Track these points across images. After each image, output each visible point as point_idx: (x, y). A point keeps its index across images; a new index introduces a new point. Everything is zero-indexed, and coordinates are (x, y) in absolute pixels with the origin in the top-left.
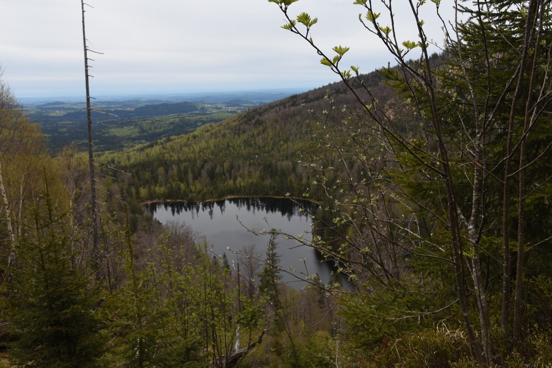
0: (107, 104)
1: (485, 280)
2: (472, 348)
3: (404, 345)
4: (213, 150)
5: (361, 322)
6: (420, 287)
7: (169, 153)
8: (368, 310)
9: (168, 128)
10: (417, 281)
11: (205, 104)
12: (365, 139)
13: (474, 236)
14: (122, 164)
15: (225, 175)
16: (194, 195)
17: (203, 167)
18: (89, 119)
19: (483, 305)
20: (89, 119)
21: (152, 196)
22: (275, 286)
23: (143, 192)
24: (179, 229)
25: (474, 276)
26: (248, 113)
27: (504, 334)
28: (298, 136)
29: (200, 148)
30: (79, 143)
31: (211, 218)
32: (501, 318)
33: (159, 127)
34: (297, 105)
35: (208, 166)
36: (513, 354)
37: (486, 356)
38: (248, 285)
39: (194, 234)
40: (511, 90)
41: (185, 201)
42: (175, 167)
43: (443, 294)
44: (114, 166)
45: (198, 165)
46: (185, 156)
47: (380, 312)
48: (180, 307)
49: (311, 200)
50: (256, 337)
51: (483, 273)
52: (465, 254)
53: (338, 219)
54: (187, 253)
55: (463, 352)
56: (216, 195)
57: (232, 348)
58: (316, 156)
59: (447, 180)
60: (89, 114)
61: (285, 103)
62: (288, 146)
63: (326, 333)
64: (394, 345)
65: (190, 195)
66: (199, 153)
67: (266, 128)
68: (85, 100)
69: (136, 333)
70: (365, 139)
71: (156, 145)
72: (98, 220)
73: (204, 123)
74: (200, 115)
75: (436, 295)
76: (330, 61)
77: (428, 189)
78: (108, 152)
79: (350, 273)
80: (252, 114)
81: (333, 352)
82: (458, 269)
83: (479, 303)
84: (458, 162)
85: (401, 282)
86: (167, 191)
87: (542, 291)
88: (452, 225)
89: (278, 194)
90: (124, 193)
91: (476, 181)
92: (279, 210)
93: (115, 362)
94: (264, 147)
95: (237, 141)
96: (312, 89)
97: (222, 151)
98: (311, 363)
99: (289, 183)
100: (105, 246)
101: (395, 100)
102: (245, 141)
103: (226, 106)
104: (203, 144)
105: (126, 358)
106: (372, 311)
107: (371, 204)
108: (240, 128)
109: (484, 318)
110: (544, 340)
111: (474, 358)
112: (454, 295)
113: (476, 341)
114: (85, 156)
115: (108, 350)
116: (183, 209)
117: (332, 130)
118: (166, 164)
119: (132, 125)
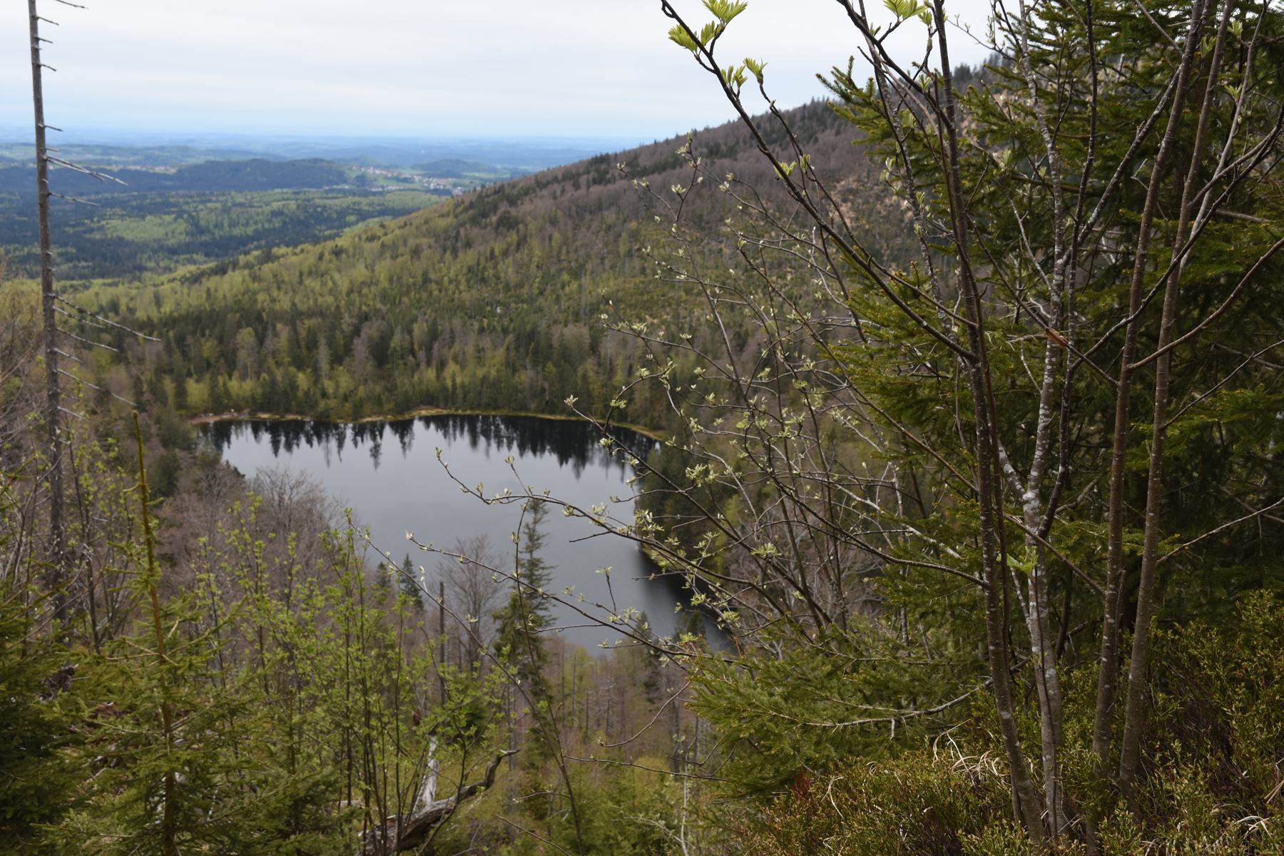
0: (98, 151)
1: (1059, 635)
2: (1019, 800)
3: (849, 791)
4: (384, 290)
5: (748, 728)
6: (897, 648)
7: (268, 290)
8: (765, 698)
9: (267, 225)
10: (890, 635)
11: (368, 166)
12: (779, 277)
13: (1037, 519)
14: (141, 315)
15: (414, 356)
16: (333, 403)
17: (357, 331)
18: (43, 185)
19: (1051, 692)
20: (43, 185)
21: (218, 402)
22: (535, 642)
23: (197, 390)
24: (288, 491)
25: (1031, 620)
26: (480, 197)
27: (1098, 766)
28: (607, 263)
29: (351, 282)
30: (17, 253)
31: (376, 464)
32: (1093, 725)
33: (242, 221)
34: (609, 181)
35: (371, 331)
36: (1116, 816)
37: (1051, 819)
38: (465, 638)
39: (329, 505)
40: (1144, 152)
41: (307, 419)
42: (283, 331)
43: (953, 667)
44: (117, 319)
45: (344, 327)
46: (311, 302)
47: (794, 705)
48: (282, 690)
49: (635, 428)
50: (478, 771)
51: (1053, 616)
52: (1011, 561)
53: (699, 468)
54: (308, 554)
55: (996, 810)
56: (391, 405)
57: (414, 798)
58: (651, 316)
59: (978, 369)
60: (43, 171)
61: (579, 175)
62: (580, 286)
63: (659, 764)
64: (828, 792)
65: (322, 404)
66: (348, 294)
67: (525, 237)
68: (33, 138)
69: (159, 758)
70: (779, 277)
71: (234, 269)
72: (65, 460)
73: (363, 216)
74: (354, 194)
75: (935, 668)
76: (693, 37)
77: (931, 400)
78: (100, 281)
79: (724, 609)
80: (490, 199)
81: (675, 811)
82: (993, 599)
83: (1040, 688)
84: (1008, 331)
85: (850, 635)
86: (260, 390)
87: (1194, 661)
88: (984, 487)
89: (551, 407)
90: (142, 393)
91: (1047, 380)
92: (553, 450)
93: (96, 834)
94: (520, 285)
95: (449, 268)
96: (650, 142)
97: (408, 293)
98: (620, 838)
99: (579, 382)
100: (83, 530)
101: (858, 180)
102: (470, 270)
103: (424, 176)
104: (360, 272)
105: (128, 822)
106: (776, 703)
107: (785, 434)
108: (458, 233)
109: (1051, 726)
110: (1193, 779)
111: (1023, 824)
112: (980, 669)
113: (1028, 782)
114: (34, 287)
115: (80, 805)
116: (303, 440)
117: (695, 249)
118: (260, 322)
119: (169, 213)
